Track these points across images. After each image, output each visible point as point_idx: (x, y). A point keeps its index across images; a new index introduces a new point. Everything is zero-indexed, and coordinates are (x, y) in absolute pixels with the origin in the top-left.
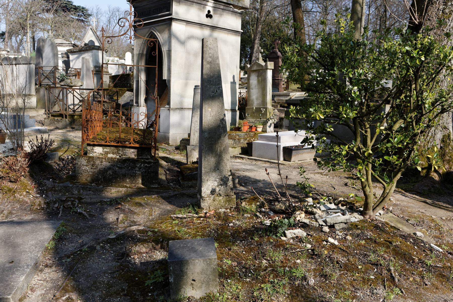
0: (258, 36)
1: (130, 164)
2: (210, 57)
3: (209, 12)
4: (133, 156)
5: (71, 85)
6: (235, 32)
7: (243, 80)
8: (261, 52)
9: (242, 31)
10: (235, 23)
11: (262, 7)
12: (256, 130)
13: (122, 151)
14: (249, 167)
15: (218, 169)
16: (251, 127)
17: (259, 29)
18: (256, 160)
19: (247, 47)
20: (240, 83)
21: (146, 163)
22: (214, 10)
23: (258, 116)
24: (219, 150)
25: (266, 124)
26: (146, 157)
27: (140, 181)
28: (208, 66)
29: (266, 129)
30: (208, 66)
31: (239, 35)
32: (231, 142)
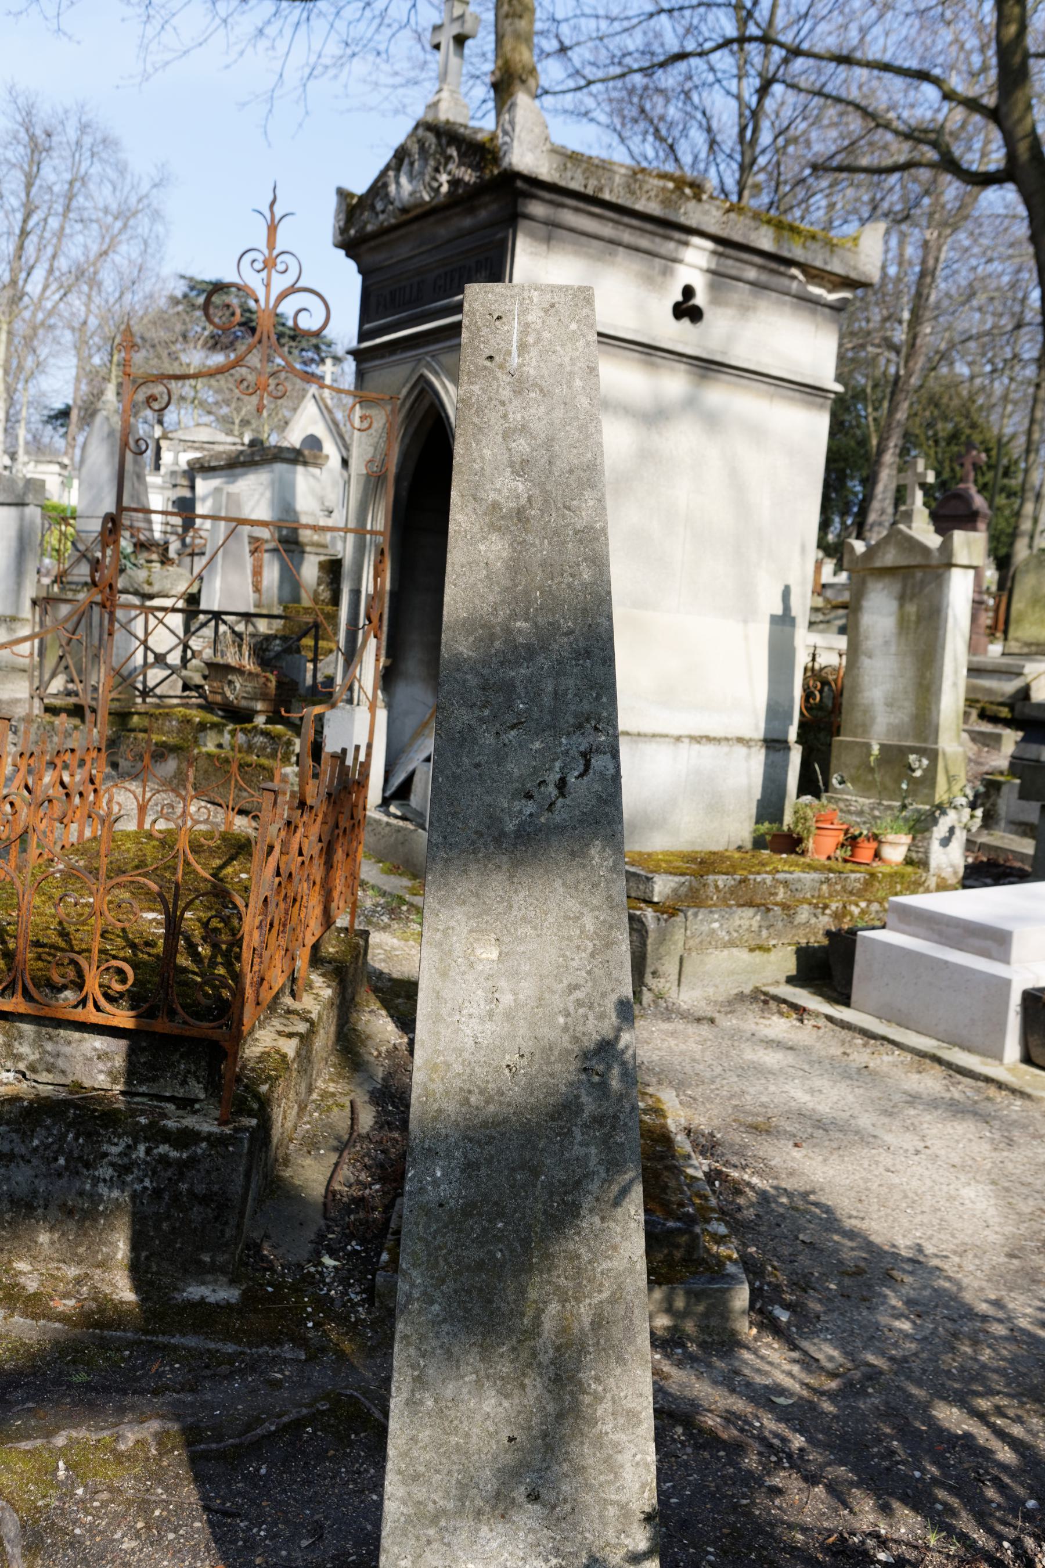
0: (894, 442)
1: (63, 1137)
2: (521, 467)
3: (688, 292)
4: (102, 1080)
5: (147, 589)
6: (811, 391)
7: (829, 593)
8: (923, 486)
9: (839, 388)
10: (805, 346)
11: (915, 337)
12: (877, 855)
13: (37, 1042)
14: (828, 1097)
15: (534, 1497)
16: (852, 841)
17: (901, 415)
18: (867, 1034)
19: (852, 478)
20: (820, 602)
21: (167, 1137)
22: (713, 287)
23: (889, 784)
24: (548, 1325)
25: (928, 829)
26: (180, 1093)
27: (121, 1248)
28: (495, 549)
29: (927, 853)
30: (495, 549)
31: (821, 407)
32: (745, 923)
